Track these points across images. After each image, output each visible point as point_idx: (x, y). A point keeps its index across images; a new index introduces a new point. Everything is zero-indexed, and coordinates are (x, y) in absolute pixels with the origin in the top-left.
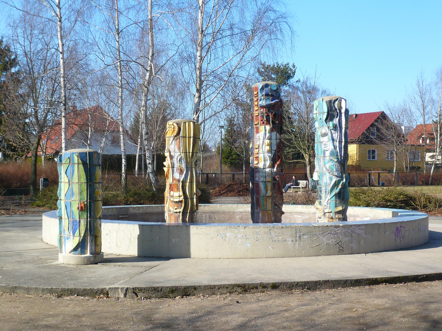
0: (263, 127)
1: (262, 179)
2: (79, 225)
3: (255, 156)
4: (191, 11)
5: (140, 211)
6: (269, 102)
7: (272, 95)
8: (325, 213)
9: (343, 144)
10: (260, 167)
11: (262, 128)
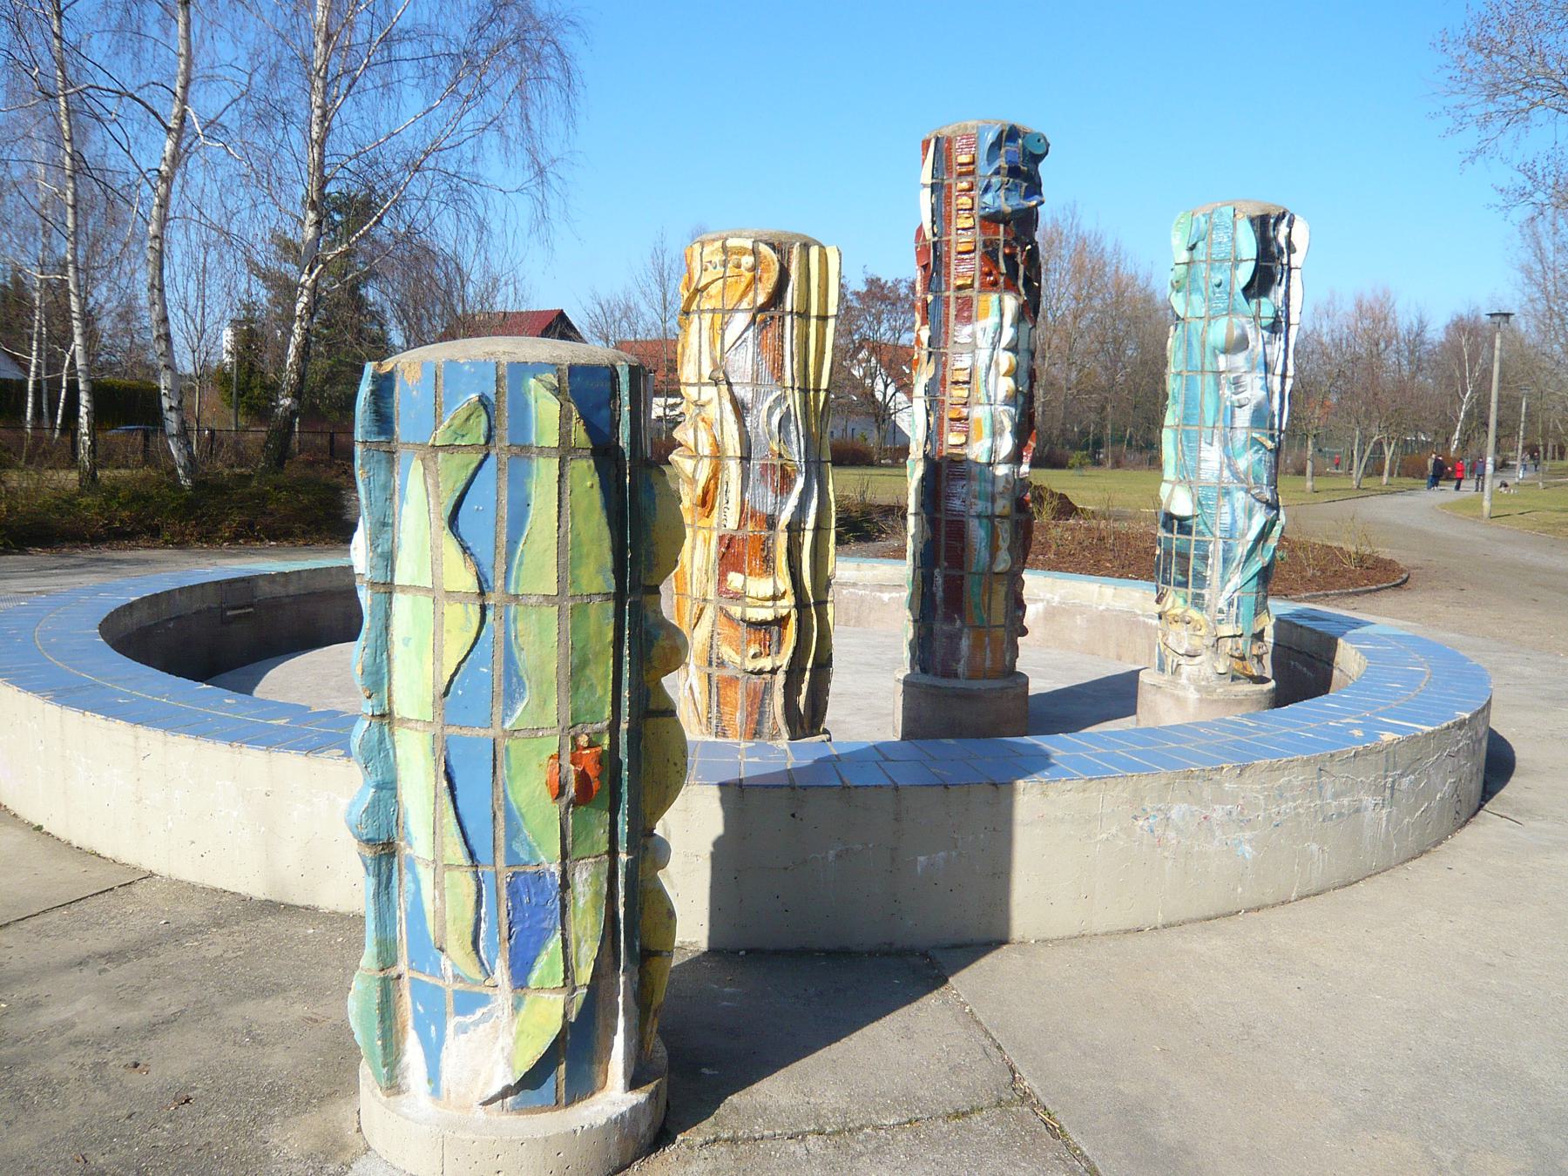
1: (980, 506)
2: (564, 907)
5: (292, 589)
10: (971, 457)
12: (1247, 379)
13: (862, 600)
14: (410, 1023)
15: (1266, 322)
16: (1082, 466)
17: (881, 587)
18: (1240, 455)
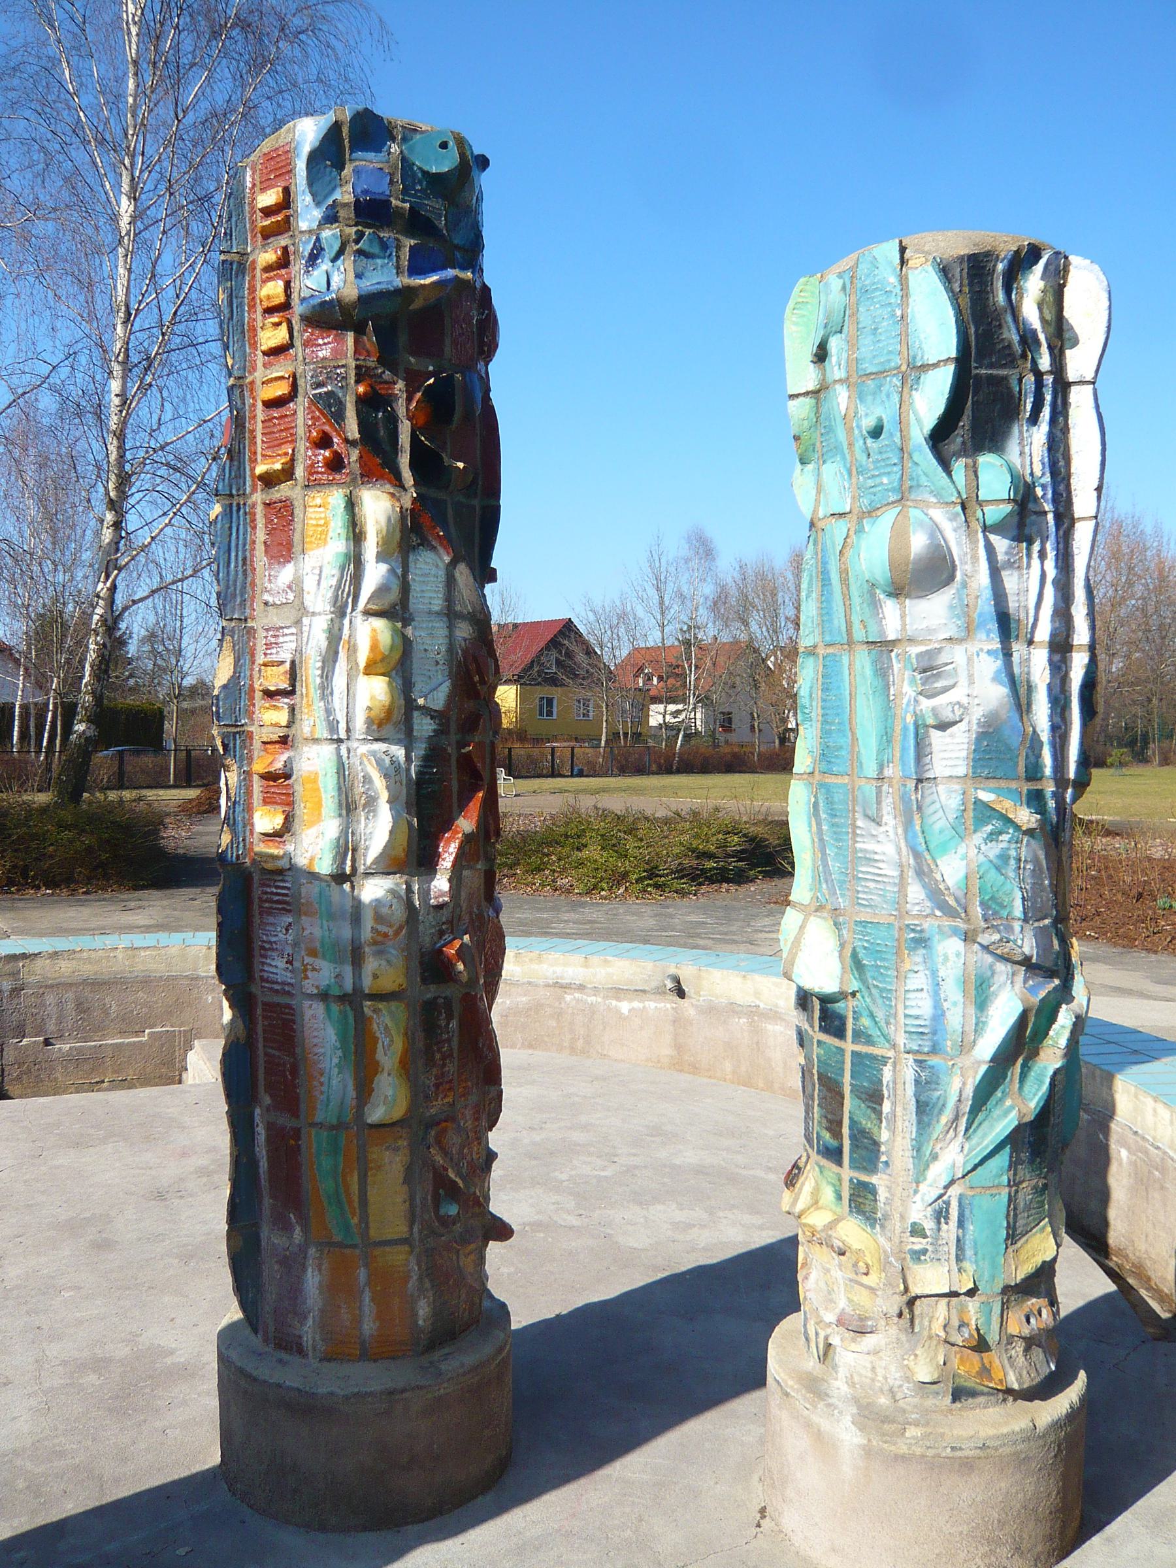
0: (336, 498)
1: (324, 974)
3: (259, 767)
6: (384, 276)
7: (417, 223)
8: (911, 1303)
10: (301, 861)
11: (323, 510)
12: (957, 655)
13: (592, 1010)
15: (995, 513)
16: (1122, 765)
17: (618, 992)
18: (944, 848)
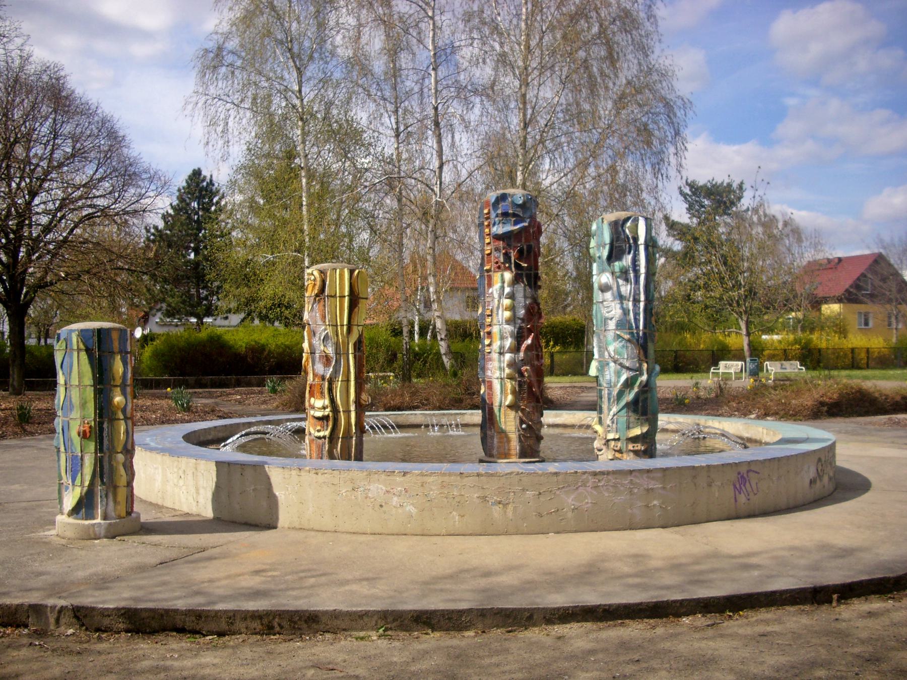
4: (334, 63)
6: (509, 228)
7: (514, 215)
9: (642, 305)
14: (406, 435)
